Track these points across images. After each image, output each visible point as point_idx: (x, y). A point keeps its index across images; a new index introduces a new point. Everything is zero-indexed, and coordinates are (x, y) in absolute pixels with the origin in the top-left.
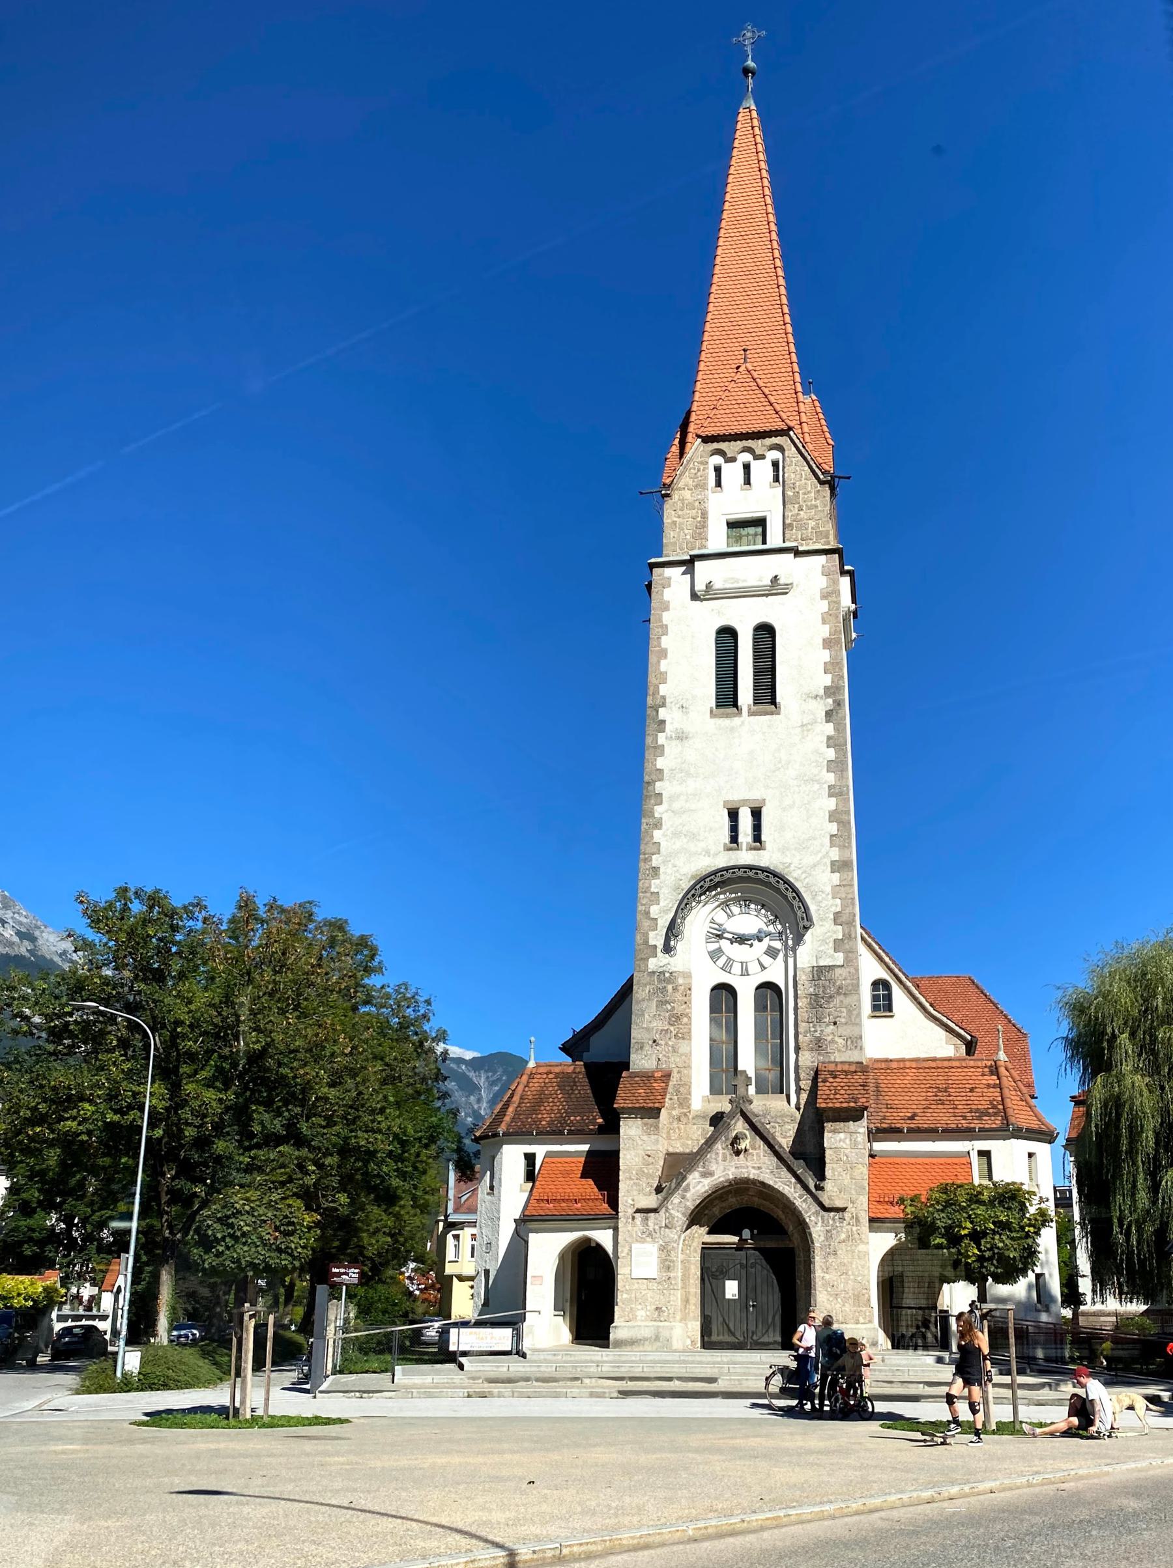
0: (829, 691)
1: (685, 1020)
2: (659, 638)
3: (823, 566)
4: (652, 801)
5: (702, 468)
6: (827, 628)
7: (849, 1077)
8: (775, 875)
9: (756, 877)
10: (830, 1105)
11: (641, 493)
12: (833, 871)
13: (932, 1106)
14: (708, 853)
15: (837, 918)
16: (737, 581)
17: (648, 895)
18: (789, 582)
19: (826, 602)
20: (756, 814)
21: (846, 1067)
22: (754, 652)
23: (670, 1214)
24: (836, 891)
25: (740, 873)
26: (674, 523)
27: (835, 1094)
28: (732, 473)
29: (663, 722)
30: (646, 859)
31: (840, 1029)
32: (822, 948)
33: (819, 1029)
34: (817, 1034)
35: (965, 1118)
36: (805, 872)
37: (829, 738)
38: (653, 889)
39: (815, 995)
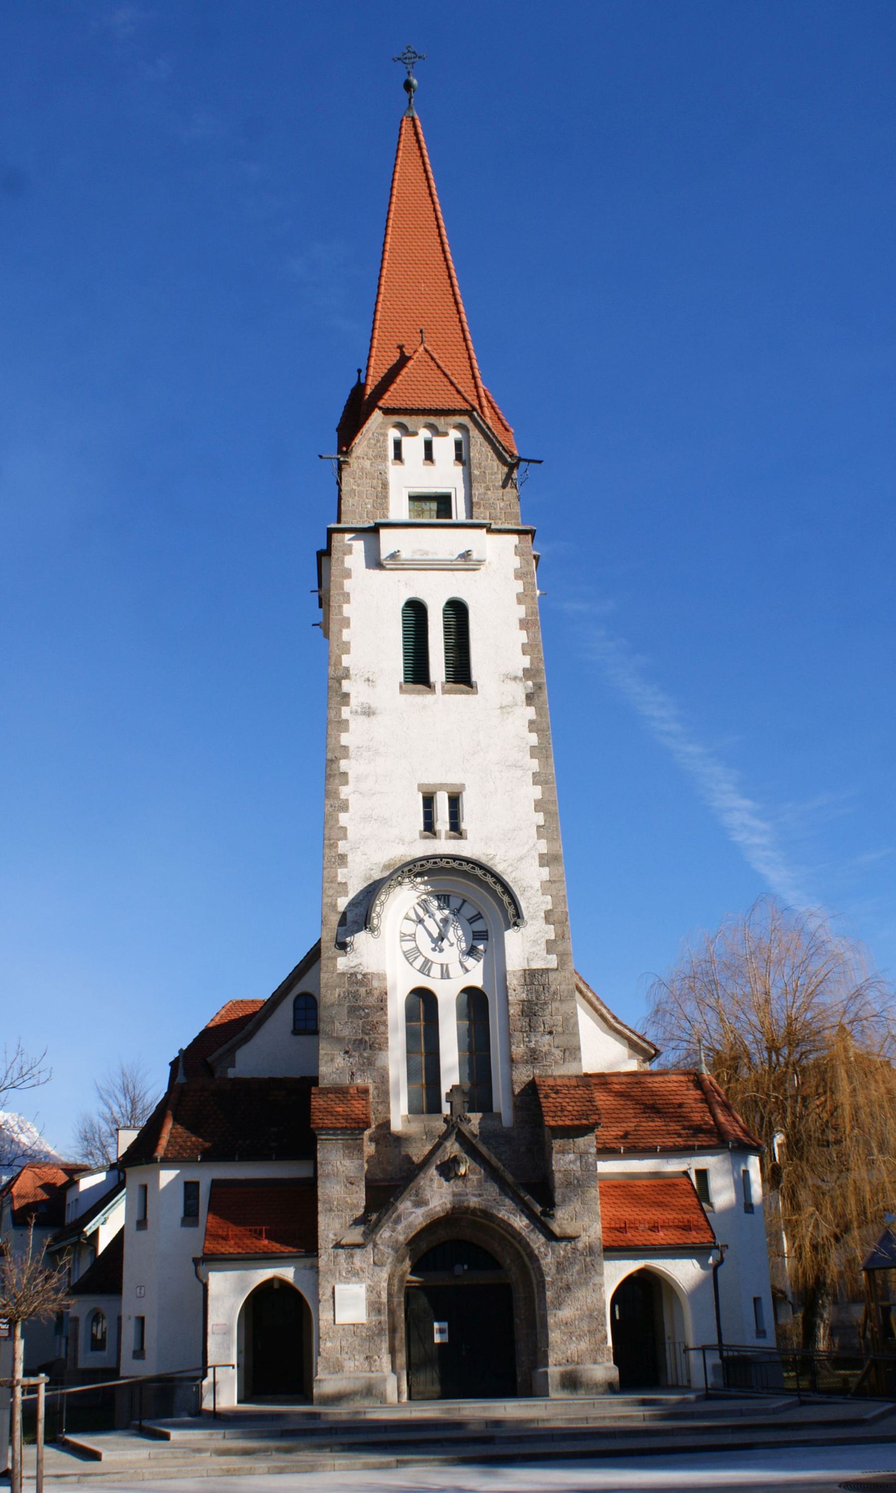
0: (528, 673)
1: (382, 1028)
2: (340, 607)
3: (516, 547)
4: (337, 781)
5: (381, 439)
6: (523, 608)
7: (572, 1092)
8: (482, 867)
9: (460, 868)
10: (560, 1123)
11: (321, 457)
12: (542, 865)
13: (643, 1124)
14: (402, 841)
15: (548, 917)
16: (427, 553)
17: (335, 885)
18: (482, 559)
19: (520, 583)
20: (455, 801)
21: (566, 1082)
22: (445, 628)
23: (379, 1249)
24: (547, 886)
25: (443, 864)
26: (353, 491)
27: (562, 1111)
28: (413, 447)
29: (347, 695)
30: (331, 845)
31: (556, 1040)
32: (533, 950)
33: (533, 1039)
34: (532, 1045)
35: (680, 1135)
36: (511, 865)
37: (531, 722)
38: (340, 879)
39: (528, 1001)
